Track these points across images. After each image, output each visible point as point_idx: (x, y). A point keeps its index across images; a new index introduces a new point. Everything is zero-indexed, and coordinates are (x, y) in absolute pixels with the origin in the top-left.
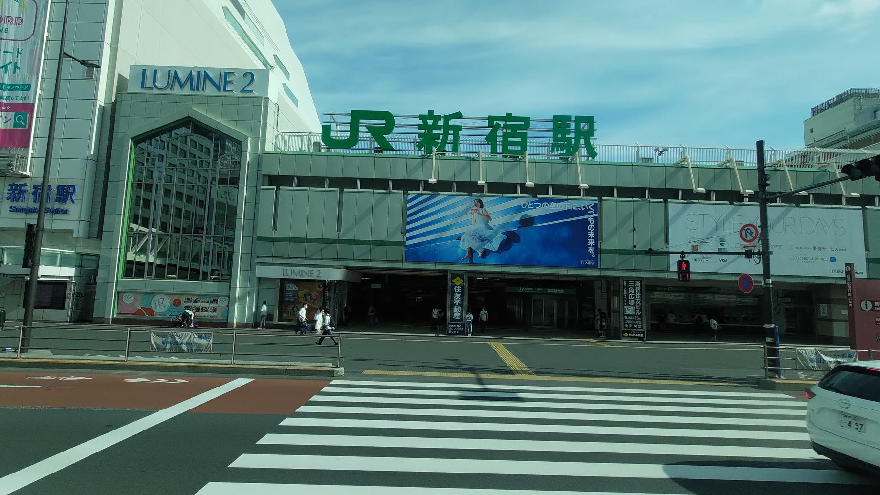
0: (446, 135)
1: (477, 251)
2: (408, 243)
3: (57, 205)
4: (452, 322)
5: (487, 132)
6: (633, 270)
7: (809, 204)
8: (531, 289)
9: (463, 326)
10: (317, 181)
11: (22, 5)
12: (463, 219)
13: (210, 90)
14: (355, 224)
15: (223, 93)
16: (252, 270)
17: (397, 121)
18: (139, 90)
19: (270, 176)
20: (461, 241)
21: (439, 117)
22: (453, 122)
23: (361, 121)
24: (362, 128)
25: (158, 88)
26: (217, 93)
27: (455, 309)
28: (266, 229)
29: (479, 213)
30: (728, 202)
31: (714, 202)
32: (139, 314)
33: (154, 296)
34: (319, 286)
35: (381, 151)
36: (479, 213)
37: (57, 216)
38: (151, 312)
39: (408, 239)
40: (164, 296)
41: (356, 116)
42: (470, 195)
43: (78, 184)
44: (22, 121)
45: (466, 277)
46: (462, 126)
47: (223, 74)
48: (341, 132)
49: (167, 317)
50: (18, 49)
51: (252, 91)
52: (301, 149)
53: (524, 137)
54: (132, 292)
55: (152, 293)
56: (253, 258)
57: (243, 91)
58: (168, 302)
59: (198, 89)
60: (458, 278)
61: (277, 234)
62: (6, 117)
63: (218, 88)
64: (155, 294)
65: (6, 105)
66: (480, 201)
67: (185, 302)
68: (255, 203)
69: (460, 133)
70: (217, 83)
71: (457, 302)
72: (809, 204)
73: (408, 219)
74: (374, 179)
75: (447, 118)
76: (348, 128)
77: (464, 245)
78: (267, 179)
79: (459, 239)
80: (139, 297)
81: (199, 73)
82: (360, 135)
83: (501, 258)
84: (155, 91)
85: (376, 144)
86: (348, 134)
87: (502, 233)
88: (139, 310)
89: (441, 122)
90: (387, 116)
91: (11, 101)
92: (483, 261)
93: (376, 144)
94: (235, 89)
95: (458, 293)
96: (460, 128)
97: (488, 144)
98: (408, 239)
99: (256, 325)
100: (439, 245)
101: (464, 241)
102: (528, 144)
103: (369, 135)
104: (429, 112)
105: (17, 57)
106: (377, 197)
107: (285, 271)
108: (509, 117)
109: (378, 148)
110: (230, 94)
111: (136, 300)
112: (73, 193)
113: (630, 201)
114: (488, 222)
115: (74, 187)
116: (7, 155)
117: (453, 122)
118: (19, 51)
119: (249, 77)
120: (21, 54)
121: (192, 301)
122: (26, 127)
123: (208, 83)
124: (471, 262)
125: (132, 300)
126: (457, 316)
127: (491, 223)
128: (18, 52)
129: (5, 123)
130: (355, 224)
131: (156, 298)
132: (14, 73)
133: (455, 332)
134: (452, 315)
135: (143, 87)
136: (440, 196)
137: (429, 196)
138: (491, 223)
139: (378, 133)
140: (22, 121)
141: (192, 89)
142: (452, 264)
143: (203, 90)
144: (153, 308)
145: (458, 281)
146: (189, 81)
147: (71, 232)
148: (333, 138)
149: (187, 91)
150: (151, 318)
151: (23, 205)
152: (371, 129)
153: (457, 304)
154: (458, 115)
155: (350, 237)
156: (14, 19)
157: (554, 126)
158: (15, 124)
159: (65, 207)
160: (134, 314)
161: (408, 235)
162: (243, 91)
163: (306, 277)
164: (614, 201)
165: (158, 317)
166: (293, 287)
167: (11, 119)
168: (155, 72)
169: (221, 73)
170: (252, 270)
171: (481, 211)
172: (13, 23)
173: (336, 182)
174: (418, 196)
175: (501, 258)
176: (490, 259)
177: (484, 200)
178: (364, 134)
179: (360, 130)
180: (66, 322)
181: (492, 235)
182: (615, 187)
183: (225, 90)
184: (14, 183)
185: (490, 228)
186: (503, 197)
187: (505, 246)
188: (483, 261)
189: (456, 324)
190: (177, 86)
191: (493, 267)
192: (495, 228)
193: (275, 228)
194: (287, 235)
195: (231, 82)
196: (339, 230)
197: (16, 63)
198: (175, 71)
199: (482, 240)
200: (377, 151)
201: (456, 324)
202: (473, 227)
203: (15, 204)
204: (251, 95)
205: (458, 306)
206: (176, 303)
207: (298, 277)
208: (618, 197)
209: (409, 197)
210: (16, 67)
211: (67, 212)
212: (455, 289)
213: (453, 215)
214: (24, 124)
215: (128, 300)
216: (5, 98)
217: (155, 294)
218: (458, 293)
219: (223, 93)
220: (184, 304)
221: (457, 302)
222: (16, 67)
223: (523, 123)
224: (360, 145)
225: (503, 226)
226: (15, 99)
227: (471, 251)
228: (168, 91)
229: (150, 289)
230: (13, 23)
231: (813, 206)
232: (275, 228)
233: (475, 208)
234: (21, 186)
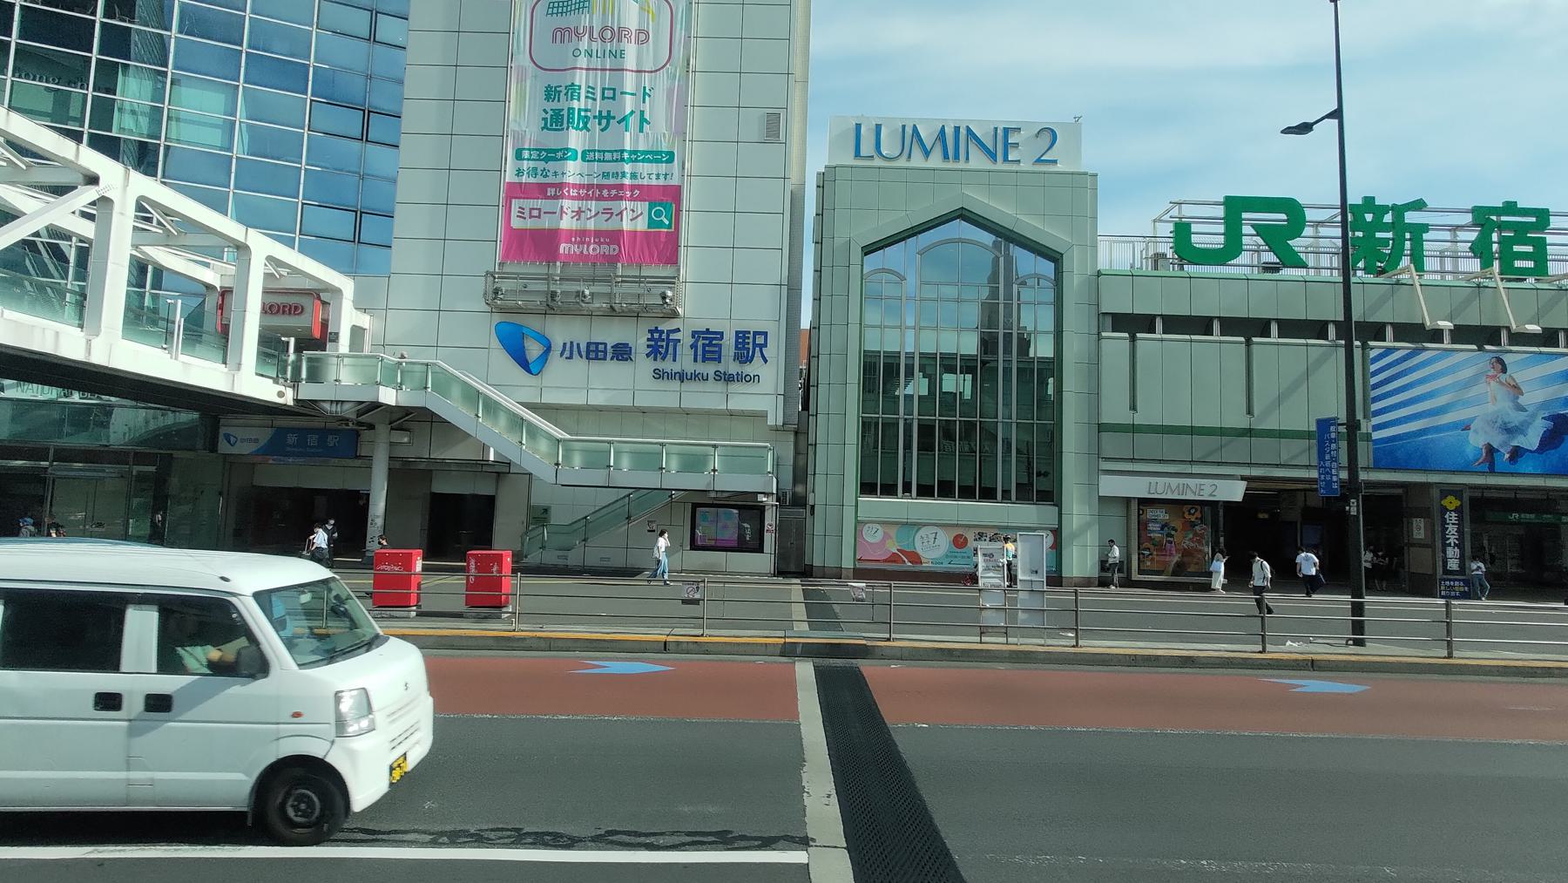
0: (1398, 241)
1: (1501, 450)
2: (1376, 435)
3: (734, 368)
4: (1445, 577)
5: (1473, 236)
6: (1250, 465)
7: (1443, 343)
8: (1533, 516)
9: (1466, 582)
10: (1202, 325)
11: (647, 8)
12: (1473, 392)
13: (978, 161)
14: (1279, 400)
15: (1000, 166)
16: (1093, 485)
17: (1310, 215)
18: (850, 160)
19: (1114, 315)
20: (1471, 430)
21: (1385, 209)
22: (558, 89)
23: (1245, 215)
24: (1247, 229)
25: (884, 156)
26: (989, 165)
27: (1450, 552)
28: (1115, 411)
29: (1501, 382)
30: (1475, 347)
31: (1159, 336)
32: (895, 561)
33: (920, 528)
34: (1189, 511)
35: (1276, 270)
36: (1501, 382)
37: (734, 387)
38: (915, 558)
39: (1377, 428)
40: (935, 529)
41: (1235, 207)
42: (1481, 349)
43: (770, 328)
44: (663, 218)
45: (1466, 496)
46: (1428, 225)
47: (1000, 132)
48: (1208, 236)
49: (945, 566)
50: (645, 88)
51: (1055, 162)
52: (1132, 266)
53: (1540, 245)
54: (879, 523)
55: (914, 524)
56: (1097, 458)
57: (1039, 161)
58: (944, 540)
59: (957, 157)
60: (1451, 498)
61: (1140, 419)
62: (633, 211)
63: (992, 156)
64: (919, 526)
65: (633, 187)
66: (1500, 361)
67: (975, 540)
68: (1095, 365)
69: (1425, 236)
70: (990, 145)
71: (1452, 540)
72: (1443, 343)
73: (1374, 394)
74: (1190, 317)
75: (1399, 211)
76: (1221, 229)
77: (1476, 441)
78: (1109, 320)
79: (1467, 428)
80: (893, 531)
81: (957, 129)
82: (1245, 240)
83: (1545, 461)
84: (878, 162)
85: (1270, 257)
86: (1221, 239)
87: (1543, 418)
88: (894, 553)
89: (1388, 218)
90: (1291, 207)
91: (640, 182)
92: (1513, 468)
93: (1270, 257)
94: (1023, 157)
95: (1453, 524)
96: (1425, 228)
97: (1475, 257)
98: (1377, 428)
99: (1104, 583)
100: (1432, 439)
101: (1476, 432)
102: (1549, 257)
103: (1259, 240)
104: (1366, 198)
105: (644, 102)
106: (1315, 353)
107: (1153, 485)
108: (1510, 208)
109: (1275, 263)
110: (1014, 167)
111: (886, 536)
112: (765, 345)
113: (1186, 341)
114: (1518, 398)
115: (765, 334)
116: (636, 277)
117: (1411, 217)
118: (647, 91)
119: (1047, 137)
120: (649, 96)
121: (988, 539)
122: (671, 228)
123: (973, 149)
124: (1492, 471)
125: (880, 535)
126: (1453, 565)
127: (1522, 400)
128: (645, 93)
129: (631, 220)
130: (1279, 400)
131: (923, 532)
132: (641, 131)
133: (1453, 594)
134: (1445, 563)
135: (857, 154)
136: (1427, 352)
137: (1409, 351)
138: (1522, 400)
139: (1275, 238)
140: (663, 218)
141: (946, 157)
142: (1453, 472)
143: (967, 159)
144: (919, 551)
145: (1451, 502)
146: (1042, 158)
147: (763, 415)
148: (1197, 246)
149: (935, 161)
150: (918, 568)
151: (676, 367)
152: (1260, 230)
153: (1452, 545)
154: (1419, 205)
155: (1271, 424)
156: (634, 34)
157: (1549, 219)
158: (651, 223)
159: (749, 369)
160: (885, 561)
161: (1376, 421)
162: (1039, 161)
163: (1190, 497)
164: (1215, 342)
165: (927, 565)
166: (1161, 514)
167: (642, 213)
168: (878, 127)
169: (996, 129)
170: (1093, 485)
171: (1503, 377)
172: (633, 41)
173: (1231, 326)
174: (1389, 351)
175: (1545, 461)
176: (1525, 465)
177: (1507, 358)
178: (1250, 239)
179: (1192, 230)
180: (766, 575)
181: (1525, 421)
182: (1503, 327)
183: (1006, 159)
184: (657, 328)
185: (1521, 408)
186: (1541, 353)
187: (1550, 440)
188: (1513, 468)
189: (1455, 580)
190: (917, 153)
191: (1528, 479)
192: (1531, 409)
193: (1133, 407)
194: (1156, 421)
195: (1016, 145)
196: (1250, 412)
197: (642, 112)
198: (915, 126)
199: (1509, 430)
200: (1270, 268)
201: (1456, 580)
202: (1490, 408)
203: (661, 365)
204: (1052, 168)
205: (1454, 548)
206: (960, 542)
207: (1176, 496)
208: (1394, 341)
209: (1373, 354)
210: (643, 120)
211: (755, 379)
212: (1447, 516)
213: (1453, 384)
214: (667, 223)
215: (873, 535)
216: (628, 175)
217: (919, 526)
218: (1453, 524)
219: (1000, 166)
220: (972, 544)
221: (1452, 540)
222: (643, 120)
223: (1534, 219)
224: (1244, 258)
225: (1544, 405)
226: (647, 176)
227: (1491, 450)
228: (902, 163)
229: (913, 518)
230: (633, 41)
231: (1450, 346)
232: (1133, 407)
233: (1492, 372)
234: (670, 332)
